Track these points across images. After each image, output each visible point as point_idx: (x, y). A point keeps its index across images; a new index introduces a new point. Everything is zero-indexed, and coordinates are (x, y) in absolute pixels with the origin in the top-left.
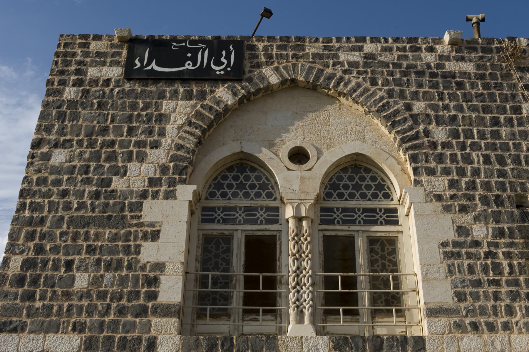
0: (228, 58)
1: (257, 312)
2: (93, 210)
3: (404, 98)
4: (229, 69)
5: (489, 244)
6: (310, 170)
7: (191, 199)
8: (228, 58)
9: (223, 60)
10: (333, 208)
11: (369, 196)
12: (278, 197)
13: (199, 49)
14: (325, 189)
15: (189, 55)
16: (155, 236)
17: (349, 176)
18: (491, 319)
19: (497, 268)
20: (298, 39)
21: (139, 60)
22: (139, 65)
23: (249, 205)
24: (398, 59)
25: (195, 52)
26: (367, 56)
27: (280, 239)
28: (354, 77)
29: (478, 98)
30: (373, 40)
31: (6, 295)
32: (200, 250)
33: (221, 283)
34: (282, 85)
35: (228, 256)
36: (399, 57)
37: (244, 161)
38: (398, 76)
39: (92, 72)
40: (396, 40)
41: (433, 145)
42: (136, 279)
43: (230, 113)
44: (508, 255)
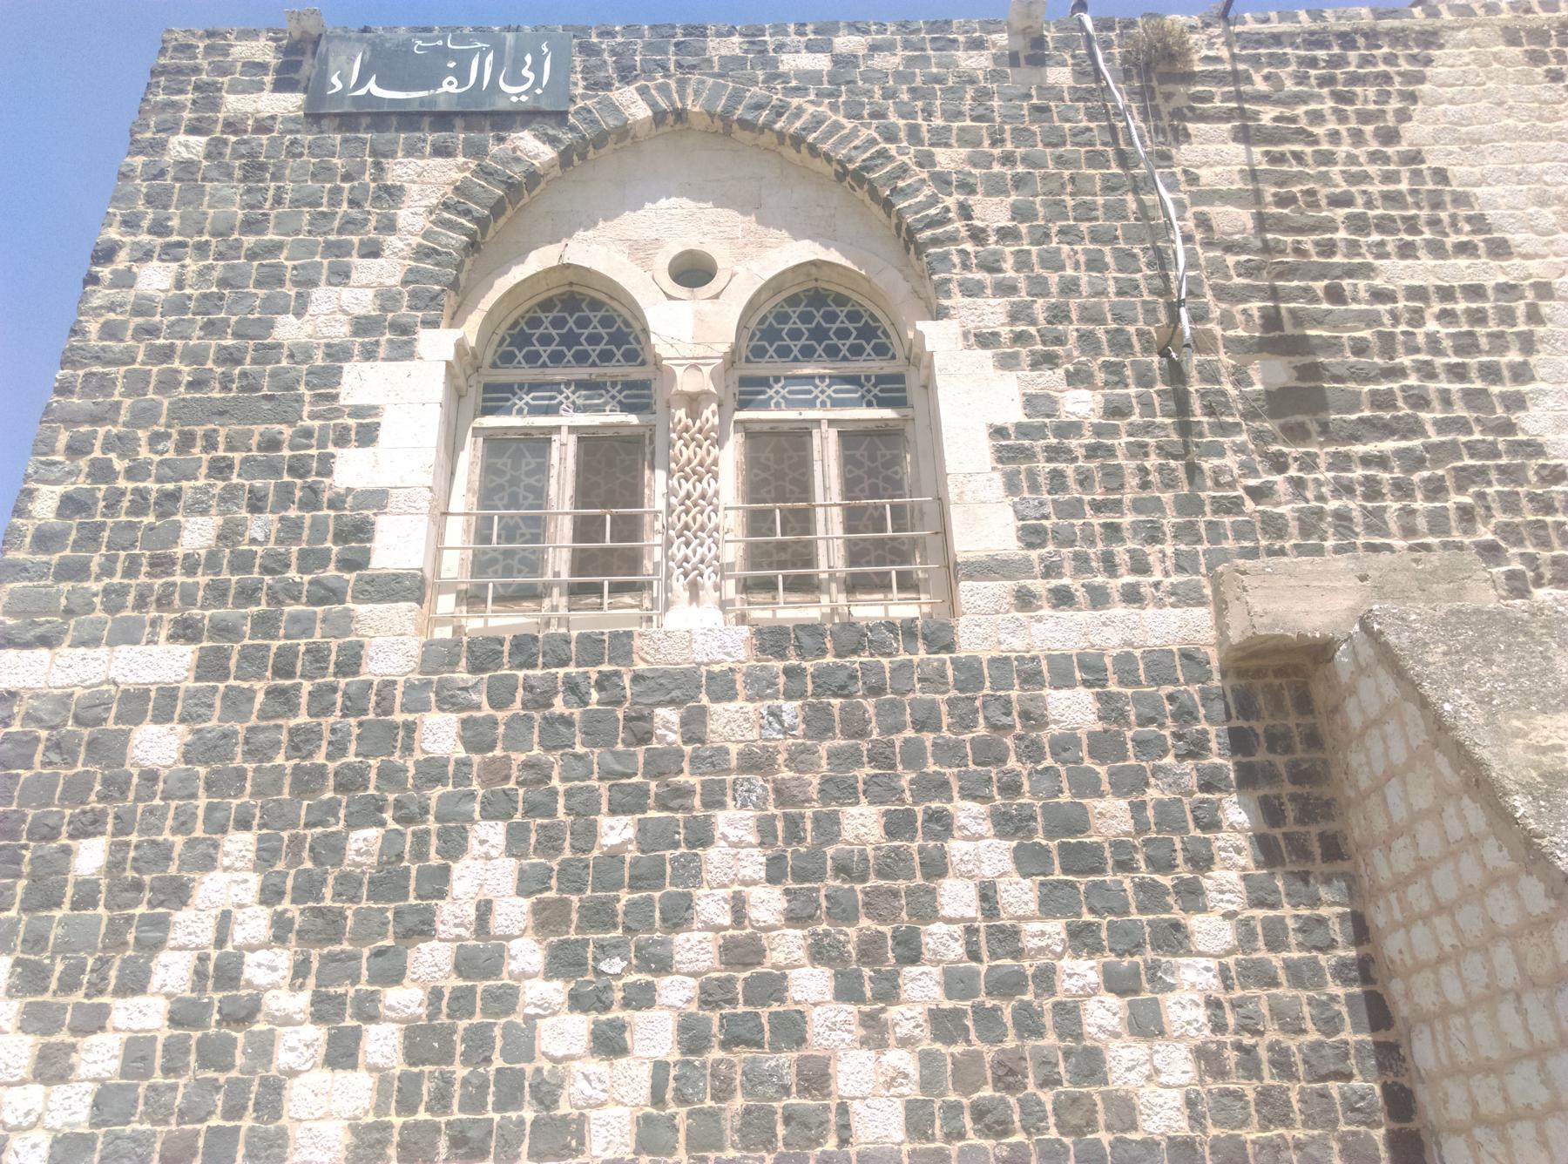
0: (537, 68)
1: (596, 589)
2: (225, 388)
3: (920, 142)
4: (539, 91)
5: (1098, 431)
6: (717, 296)
7: (451, 357)
8: (537, 68)
9: (526, 72)
10: (767, 379)
11: (844, 351)
12: (650, 359)
13: (472, 52)
14: (751, 339)
15: (452, 65)
16: (368, 436)
17: (802, 313)
18: (1100, 579)
19: (1114, 477)
20: (689, 31)
21: (339, 77)
22: (339, 86)
23: (586, 377)
24: (906, 66)
25: (464, 60)
26: (839, 61)
27: (652, 441)
28: (811, 102)
29: (1078, 139)
30: (855, 28)
31: (20, 570)
32: (478, 471)
33: (523, 535)
34: (657, 126)
35: (538, 481)
36: (910, 61)
37: (575, 288)
38: (905, 97)
39: (234, 103)
40: (903, 26)
41: (978, 236)
42: (318, 527)
43: (542, 185)
44: (1139, 450)
